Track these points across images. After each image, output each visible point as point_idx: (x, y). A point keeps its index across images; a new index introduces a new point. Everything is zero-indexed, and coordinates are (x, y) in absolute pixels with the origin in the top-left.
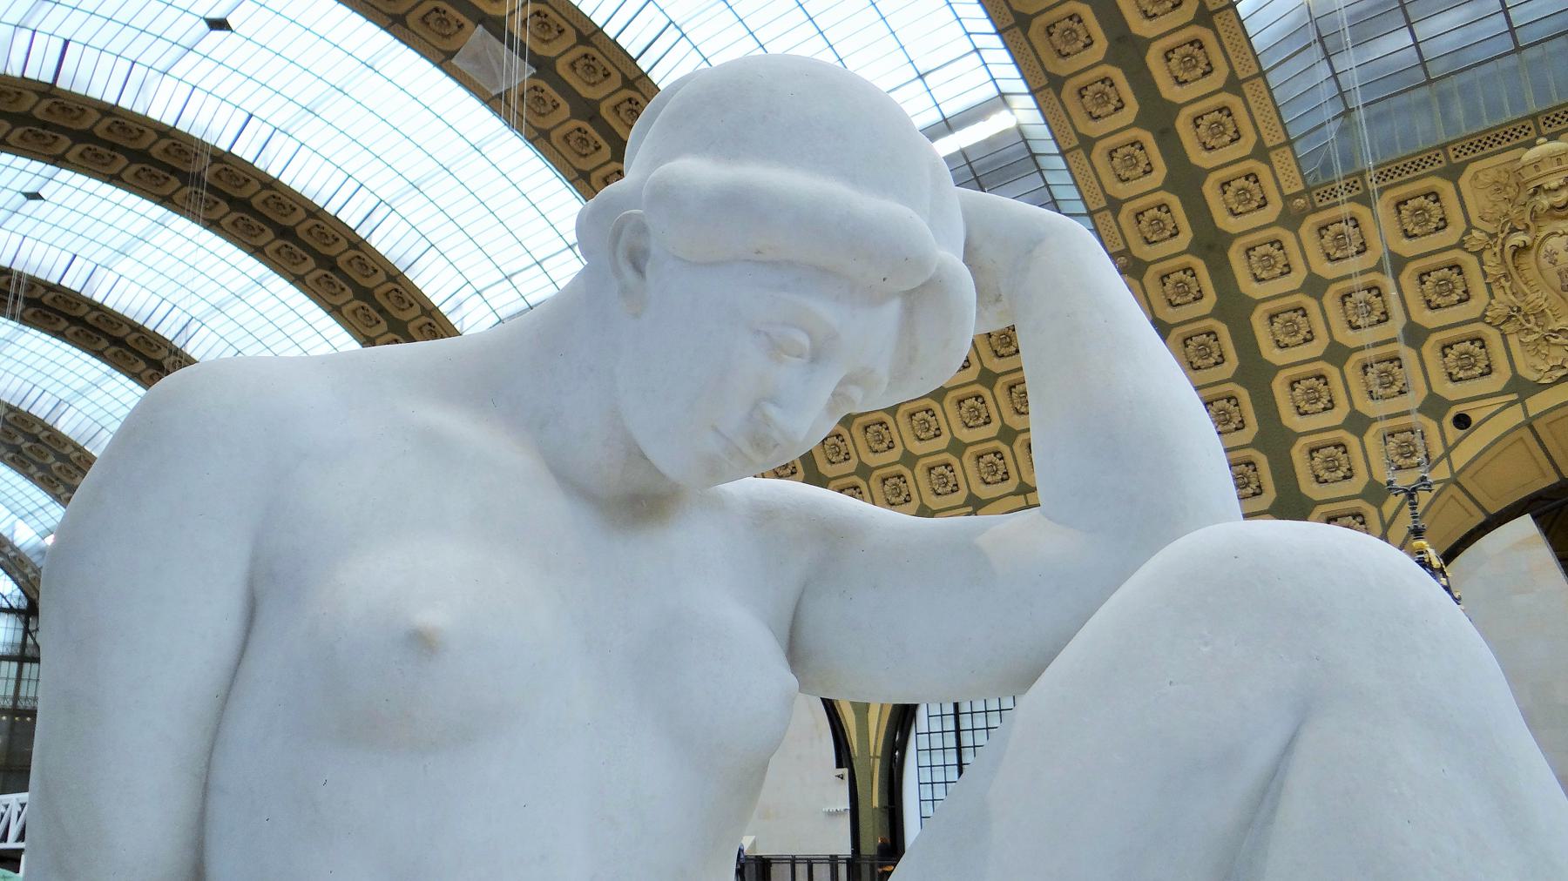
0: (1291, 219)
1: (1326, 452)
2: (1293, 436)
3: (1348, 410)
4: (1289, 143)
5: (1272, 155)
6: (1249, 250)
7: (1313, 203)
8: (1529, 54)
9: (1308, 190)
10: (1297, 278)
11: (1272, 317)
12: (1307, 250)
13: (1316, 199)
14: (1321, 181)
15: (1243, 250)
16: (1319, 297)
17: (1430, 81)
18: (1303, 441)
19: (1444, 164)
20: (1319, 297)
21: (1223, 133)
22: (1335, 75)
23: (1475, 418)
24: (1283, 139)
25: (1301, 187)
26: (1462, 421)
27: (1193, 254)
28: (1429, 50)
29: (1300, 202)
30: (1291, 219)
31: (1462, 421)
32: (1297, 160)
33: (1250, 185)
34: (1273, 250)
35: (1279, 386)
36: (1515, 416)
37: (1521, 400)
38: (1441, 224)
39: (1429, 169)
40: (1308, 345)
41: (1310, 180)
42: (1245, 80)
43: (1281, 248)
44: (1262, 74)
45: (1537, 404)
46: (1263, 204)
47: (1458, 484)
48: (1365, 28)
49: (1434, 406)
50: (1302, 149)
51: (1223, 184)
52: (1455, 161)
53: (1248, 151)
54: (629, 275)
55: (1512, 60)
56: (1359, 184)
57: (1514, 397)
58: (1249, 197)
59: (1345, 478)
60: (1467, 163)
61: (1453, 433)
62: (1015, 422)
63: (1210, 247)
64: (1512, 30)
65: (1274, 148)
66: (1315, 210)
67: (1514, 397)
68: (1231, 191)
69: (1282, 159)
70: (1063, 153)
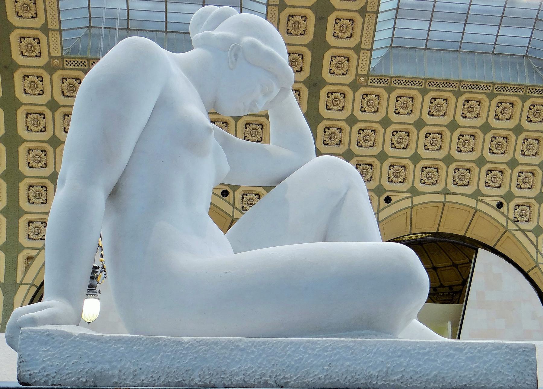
0: (50, 68)
1: (37, 188)
2: (22, 177)
3: (476, 188)
4: (60, 30)
5: (50, 33)
6: (25, 76)
7: (63, 64)
8: (170, 35)
9: (62, 57)
10: (45, 99)
11: (28, 114)
12: (354, 103)
13: (65, 63)
14: (70, 55)
15: (22, 75)
16: (53, 111)
17: (166, 31)
18: (26, 180)
19: (456, 89)
20: (53, 111)
21: (29, 11)
22: (429, 30)
23: (394, 199)
24: (58, 27)
25: (59, 54)
26: (388, 200)
27: (304, 84)
28: (171, 17)
29: (57, 62)
30: (50, 68)
31: (388, 200)
32: (61, 40)
33: (35, 43)
34: (37, 81)
35: (22, 150)
36: (407, 203)
37: (412, 197)
38: (41, 92)
39: (417, 87)
40: (42, 133)
41: (64, 53)
42: (369, 12)
43: (42, 81)
44: (377, 13)
45: (417, 200)
46: (39, 56)
47: (506, 231)
48: (414, 13)
49: (509, 196)
50: (65, 36)
51: (21, 38)
52: (528, 94)
53: (39, 26)
54: (234, 59)
55: (163, 35)
56: (86, 64)
57: (410, 195)
58: (33, 48)
59: (43, 203)
60: (499, 94)
61: (383, 204)
62: (60, 134)
63: (315, 85)
64: (166, 22)
65: (52, 30)
66: (63, 68)
67: (410, 195)
68: (24, 42)
69: (54, 36)
70: (268, 5)
